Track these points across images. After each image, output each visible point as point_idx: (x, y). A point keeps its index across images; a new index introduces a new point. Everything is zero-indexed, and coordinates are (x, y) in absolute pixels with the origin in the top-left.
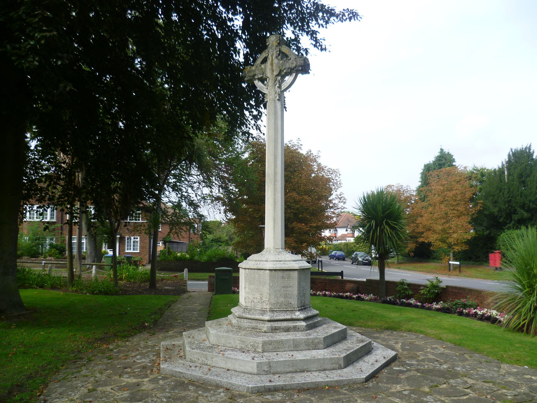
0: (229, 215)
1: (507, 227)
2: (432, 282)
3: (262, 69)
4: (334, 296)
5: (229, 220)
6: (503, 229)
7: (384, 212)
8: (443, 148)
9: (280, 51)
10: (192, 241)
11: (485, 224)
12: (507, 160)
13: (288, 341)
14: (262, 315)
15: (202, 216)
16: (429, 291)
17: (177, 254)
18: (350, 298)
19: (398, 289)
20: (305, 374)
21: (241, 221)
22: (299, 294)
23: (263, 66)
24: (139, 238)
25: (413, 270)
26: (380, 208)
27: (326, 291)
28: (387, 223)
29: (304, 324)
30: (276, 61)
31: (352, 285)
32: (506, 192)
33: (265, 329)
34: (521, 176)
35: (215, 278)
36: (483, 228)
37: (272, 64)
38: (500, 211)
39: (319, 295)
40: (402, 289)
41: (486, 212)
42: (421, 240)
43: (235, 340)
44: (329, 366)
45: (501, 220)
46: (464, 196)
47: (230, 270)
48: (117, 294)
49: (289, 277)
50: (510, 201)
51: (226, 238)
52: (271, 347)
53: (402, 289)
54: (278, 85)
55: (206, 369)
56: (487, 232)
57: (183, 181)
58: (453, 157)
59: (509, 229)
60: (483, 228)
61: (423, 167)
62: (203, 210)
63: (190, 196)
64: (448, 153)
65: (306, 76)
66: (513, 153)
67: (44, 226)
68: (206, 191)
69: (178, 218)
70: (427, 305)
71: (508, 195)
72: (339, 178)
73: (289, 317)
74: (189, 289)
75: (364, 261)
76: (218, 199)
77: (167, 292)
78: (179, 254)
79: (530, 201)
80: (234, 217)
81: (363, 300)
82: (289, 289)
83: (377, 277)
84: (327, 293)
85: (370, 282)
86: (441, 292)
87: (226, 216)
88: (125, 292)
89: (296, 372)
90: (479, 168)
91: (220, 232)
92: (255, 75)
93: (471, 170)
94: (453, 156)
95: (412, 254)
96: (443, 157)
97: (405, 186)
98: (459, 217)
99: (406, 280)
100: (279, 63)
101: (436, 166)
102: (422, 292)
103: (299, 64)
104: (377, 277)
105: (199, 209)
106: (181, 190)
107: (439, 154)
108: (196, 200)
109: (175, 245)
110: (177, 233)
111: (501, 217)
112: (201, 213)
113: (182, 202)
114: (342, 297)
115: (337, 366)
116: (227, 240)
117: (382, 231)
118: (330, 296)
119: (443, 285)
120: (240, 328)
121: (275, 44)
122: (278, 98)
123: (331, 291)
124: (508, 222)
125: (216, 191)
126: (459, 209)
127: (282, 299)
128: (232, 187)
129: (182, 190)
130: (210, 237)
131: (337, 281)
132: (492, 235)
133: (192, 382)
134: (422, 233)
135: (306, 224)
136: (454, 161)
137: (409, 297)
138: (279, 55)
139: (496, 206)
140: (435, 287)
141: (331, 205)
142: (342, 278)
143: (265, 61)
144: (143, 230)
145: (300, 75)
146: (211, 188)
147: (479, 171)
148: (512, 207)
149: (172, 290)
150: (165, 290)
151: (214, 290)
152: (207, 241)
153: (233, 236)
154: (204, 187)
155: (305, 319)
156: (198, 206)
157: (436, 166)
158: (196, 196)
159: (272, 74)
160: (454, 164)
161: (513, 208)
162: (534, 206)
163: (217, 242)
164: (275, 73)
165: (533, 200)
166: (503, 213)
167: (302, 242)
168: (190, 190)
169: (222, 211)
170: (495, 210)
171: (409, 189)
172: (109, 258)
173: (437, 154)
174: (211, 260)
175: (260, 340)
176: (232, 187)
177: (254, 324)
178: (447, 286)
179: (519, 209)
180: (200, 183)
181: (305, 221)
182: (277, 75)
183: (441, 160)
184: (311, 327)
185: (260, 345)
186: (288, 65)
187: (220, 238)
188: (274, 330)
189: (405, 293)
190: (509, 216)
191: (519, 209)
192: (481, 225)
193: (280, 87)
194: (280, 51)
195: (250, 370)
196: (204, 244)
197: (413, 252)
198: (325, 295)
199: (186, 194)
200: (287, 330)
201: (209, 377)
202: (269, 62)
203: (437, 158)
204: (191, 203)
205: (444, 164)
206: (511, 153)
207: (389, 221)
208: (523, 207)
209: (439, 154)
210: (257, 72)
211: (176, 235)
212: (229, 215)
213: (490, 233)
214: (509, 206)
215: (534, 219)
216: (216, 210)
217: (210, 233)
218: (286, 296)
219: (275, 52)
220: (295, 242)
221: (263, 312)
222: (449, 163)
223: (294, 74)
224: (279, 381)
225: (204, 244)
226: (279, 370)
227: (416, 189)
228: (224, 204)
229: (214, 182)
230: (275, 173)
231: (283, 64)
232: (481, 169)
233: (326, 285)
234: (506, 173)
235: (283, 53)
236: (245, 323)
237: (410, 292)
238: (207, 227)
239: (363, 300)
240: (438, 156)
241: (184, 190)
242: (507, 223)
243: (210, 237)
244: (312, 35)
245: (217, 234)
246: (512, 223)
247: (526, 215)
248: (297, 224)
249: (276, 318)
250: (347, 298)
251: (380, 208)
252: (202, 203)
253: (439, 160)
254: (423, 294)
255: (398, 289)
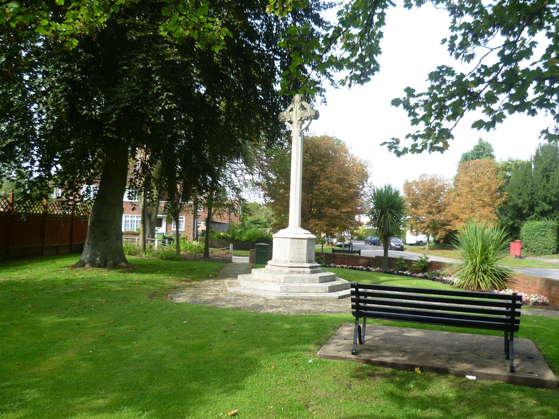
0: (268, 200)
1: (530, 218)
2: (421, 258)
3: (290, 115)
4: (350, 268)
5: (269, 203)
6: (526, 220)
7: (388, 203)
8: (482, 138)
9: (301, 105)
10: (232, 222)
11: (509, 214)
12: (535, 154)
13: (298, 277)
14: (285, 264)
15: (243, 200)
16: (418, 265)
17: (220, 233)
18: (362, 270)
19: (397, 263)
20: (306, 293)
21: (278, 205)
22: (307, 253)
23: (291, 113)
24: (184, 217)
25: (441, 256)
26: (385, 200)
27: (344, 264)
28: (390, 212)
29: (309, 270)
30: (298, 111)
31: (364, 260)
32: (530, 185)
33: (286, 271)
34: (546, 170)
35: (255, 253)
36: (508, 218)
37: (296, 113)
38: (524, 202)
39: (338, 267)
40: (401, 264)
41: (511, 204)
42: (448, 228)
43: (269, 277)
44: (320, 291)
45: (525, 211)
46: (491, 187)
47: (268, 246)
48: (179, 260)
49: (302, 243)
50: (533, 194)
51: (265, 220)
52: (289, 280)
53: (401, 264)
54: (299, 127)
55: (253, 290)
56: (512, 222)
57: (227, 168)
58: (492, 147)
59: (532, 219)
60: (508, 218)
61: (461, 156)
62: (245, 195)
63: (233, 182)
64: (487, 143)
65: (316, 121)
66: (541, 148)
67: (132, 207)
68: (248, 177)
69: (221, 201)
70: (415, 275)
71: (532, 188)
72: (370, 168)
73: (300, 266)
74: (233, 261)
75: (396, 247)
76: (258, 184)
77: (218, 261)
78: (221, 234)
79: (552, 194)
80: (273, 201)
81: (370, 271)
82: (302, 250)
83: (383, 255)
84: (344, 266)
85: (378, 258)
86: (428, 266)
87: (265, 200)
88: (185, 259)
89: (301, 292)
90: (514, 160)
91: (258, 214)
92: (285, 119)
93: (506, 161)
94: (491, 146)
95: (442, 241)
96: (481, 147)
97: (438, 175)
98: (484, 207)
99: (404, 257)
100: (300, 113)
101: (474, 155)
102: (413, 265)
103: (312, 115)
104: (382, 254)
105: (241, 194)
106: (225, 176)
107: (478, 143)
108: (239, 184)
109: (217, 225)
110: (220, 214)
111: (524, 208)
112: (243, 197)
113: (226, 187)
114: (355, 269)
115: (325, 291)
116: (265, 223)
117: (386, 217)
118: (346, 268)
119: (429, 260)
120: (272, 271)
121: (298, 100)
122: (299, 135)
123: (348, 264)
124: (531, 213)
125: (257, 178)
126: (485, 199)
127: (297, 255)
128: (271, 175)
129: (226, 175)
130: (250, 218)
131: (357, 257)
132: (516, 225)
133: (244, 296)
134: (451, 221)
135: (337, 209)
136: (492, 150)
137: (405, 269)
138: (301, 107)
139: (520, 198)
140: (423, 261)
141: (362, 193)
142: (360, 254)
143: (291, 110)
144: (190, 210)
145: (313, 121)
146: (252, 174)
147: (513, 162)
148: (535, 200)
149: (221, 260)
150: (216, 259)
151: (254, 261)
152: (246, 223)
153: (272, 219)
154: (246, 173)
155: (310, 267)
156: (241, 191)
157: (474, 155)
158: (239, 181)
159: (296, 119)
160: (492, 153)
161: (536, 201)
162: (555, 199)
163: (256, 224)
164: (299, 119)
165: (555, 193)
166: (527, 205)
167: (334, 226)
168: (233, 176)
169: (262, 196)
170: (519, 202)
171: (442, 179)
172: (160, 235)
173: (476, 143)
174: (251, 240)
175: (283, 276)
176: (271, 175)
177: (280, 269)
178: (432, 262)
179: (540, 202)
180: (242, 170)
181: (337, 207)
182: (299, 120)
183: (480, 150)
184: (312, 272)
185: (283, 279)
186: (305, 115)
187: (259, 220)
188: (292, 272)
189: (402, 266)
190: (532, 208)
191: (540, 202)
192: (506, 215)
193: (301, 128)
194: (301, 105)
195: (276, 290)
196: (243, 225)
197: (442, 239)
198: (342, 267)
199: (229, 180)
200: (299, 273)
201: (255, 293)
202: (294, 111)
203: (475, 148)
204: (234, 188)
205: (482, 154)
206: (539, 147)
207: (392, 211)
208: (545, 199)
209: (478, 143)
210: (287, 117)
211: (219, 216)
212: (268, 199)
213: (514, 224)
214: (532, 198)
215: (555, 212)
216: (257, 195)
217: (250, 215)
218: (299, 254)
219: (298, 105)
220: (327, 225)
221: (286, 262)
222: (487, 153)
223: (309, 120)
224: (290, 295)
225: (243, 225)
226: (292, 291)
227: (453, 178)
228: (264, 189)
229: (255, 170)
230: (296, 181)
231: (303, 114)
232: (516, 161)
233: (344, 260)
234: (533, 167)
235: (303, 106)
236: (276, 269)
237: (406, 266)
238: (247, 209)
239: (370, 271)
240: (476, 146)
241: (228, 176)
242: (531, 215)
243: (250, 218)
244: (329, 77)
245: (256, 216)
246: (535, 214)
247: (547, 207)
248: (328, 209)
249: (293, 266)
250: (359, 269)
251: (385, 200)
252: (244, 187)
253: (477, 150)
254: (414, 267)
255: (397, 263)
